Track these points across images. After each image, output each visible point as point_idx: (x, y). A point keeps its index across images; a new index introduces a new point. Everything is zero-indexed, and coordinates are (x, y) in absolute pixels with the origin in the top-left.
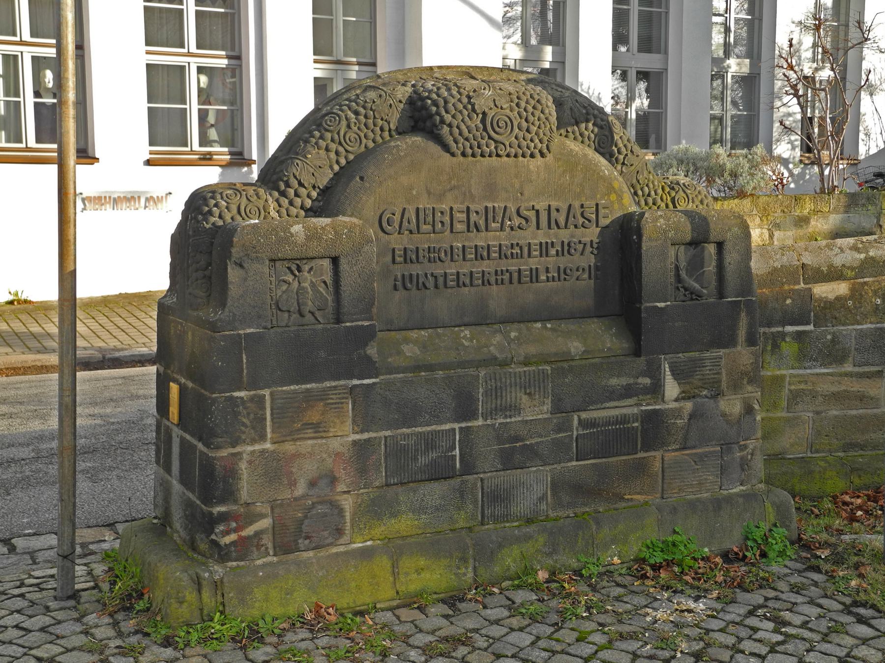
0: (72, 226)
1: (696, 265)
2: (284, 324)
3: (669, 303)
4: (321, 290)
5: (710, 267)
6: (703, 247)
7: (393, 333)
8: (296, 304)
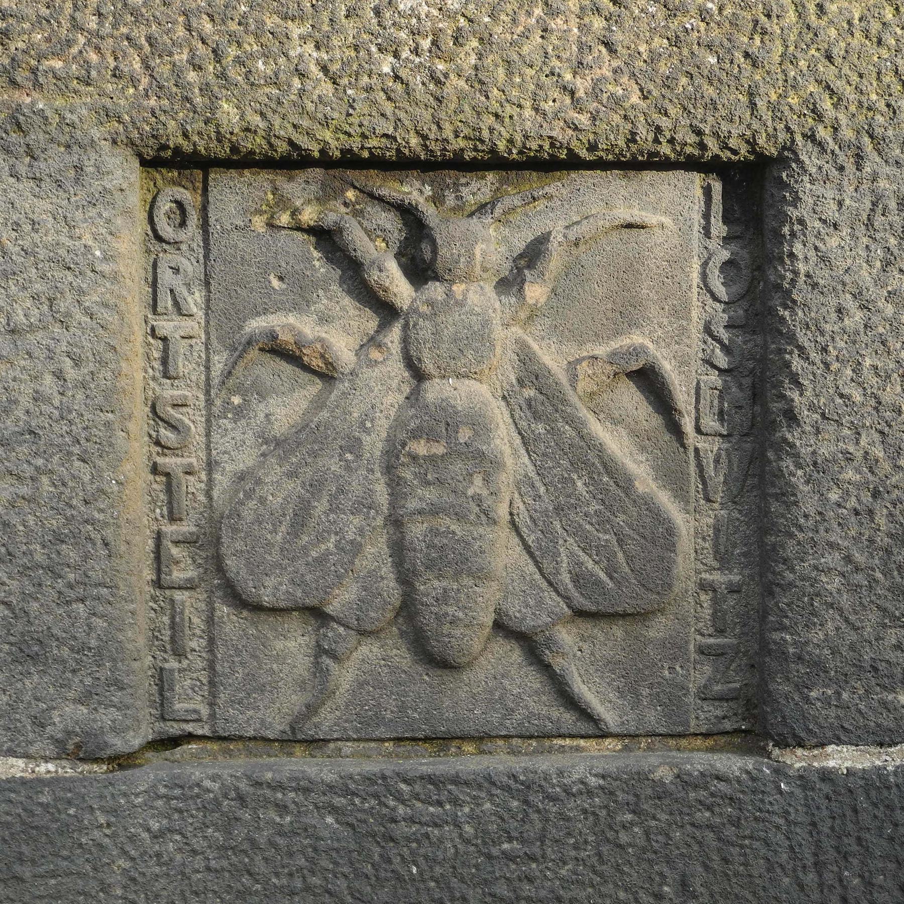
2: (277, 726)
4: (615, 443)
8: (376, 553)
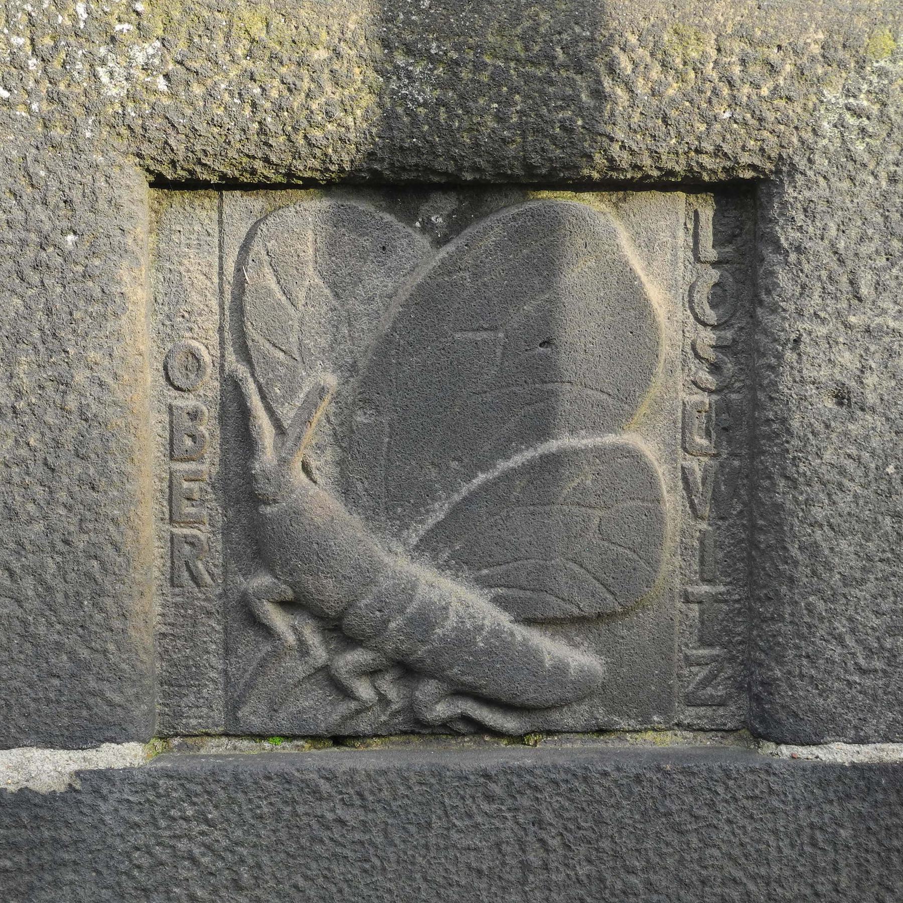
0: (227, 306)
1: (456, 407)
3: (124, 755)
5: (656, 438)
6: (551, 226)
7: (277, 351)
